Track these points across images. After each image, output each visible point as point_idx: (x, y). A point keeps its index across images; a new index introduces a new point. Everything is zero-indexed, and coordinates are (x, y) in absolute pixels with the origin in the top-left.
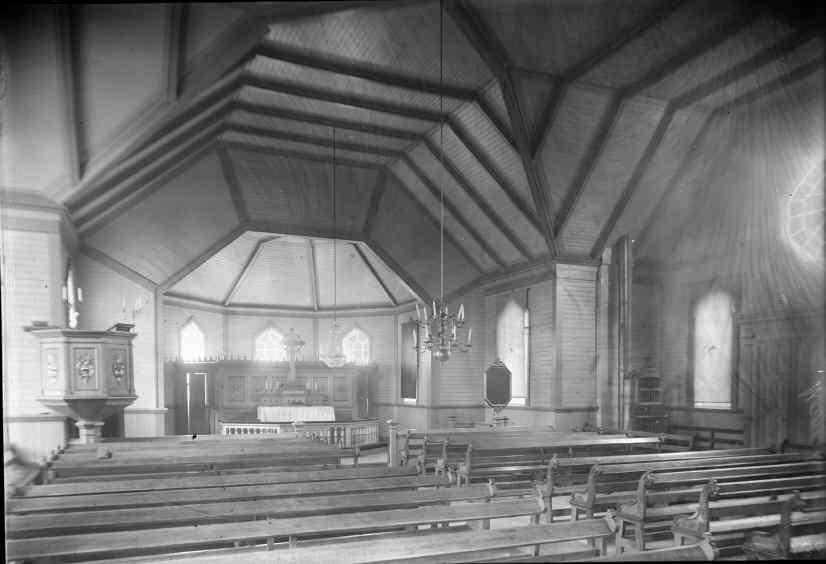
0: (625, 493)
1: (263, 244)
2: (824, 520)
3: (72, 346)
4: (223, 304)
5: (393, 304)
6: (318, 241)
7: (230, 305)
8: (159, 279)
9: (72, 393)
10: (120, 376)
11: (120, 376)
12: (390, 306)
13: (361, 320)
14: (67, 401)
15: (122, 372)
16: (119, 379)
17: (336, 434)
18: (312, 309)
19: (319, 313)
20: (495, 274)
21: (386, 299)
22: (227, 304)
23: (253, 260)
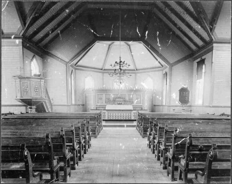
0: (206, 145)
1: (111, 46)
2: (230, 168)
3: (22, 82)
4: (102, 69)
5: (161, 66)
6: (130, 43)
7: (104, 70)
8: (67, 60)
9: (22, 97)
10: (37, 91)
11: (37, 91)
12: (161, 67)
13: (150, 74)
14: (21, 99)
15: (38, 90)
16: (37, 92)
17: (109, 115)
18: (134, 70)
19: (137, 71)
20: (198, 51)
21: (159, 65)
22: (103, 69)
23: (108, 54)
